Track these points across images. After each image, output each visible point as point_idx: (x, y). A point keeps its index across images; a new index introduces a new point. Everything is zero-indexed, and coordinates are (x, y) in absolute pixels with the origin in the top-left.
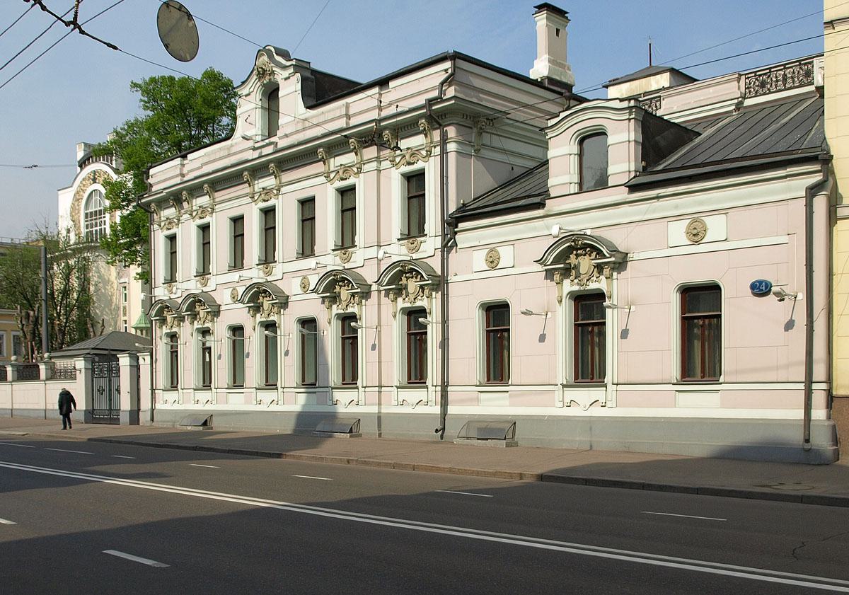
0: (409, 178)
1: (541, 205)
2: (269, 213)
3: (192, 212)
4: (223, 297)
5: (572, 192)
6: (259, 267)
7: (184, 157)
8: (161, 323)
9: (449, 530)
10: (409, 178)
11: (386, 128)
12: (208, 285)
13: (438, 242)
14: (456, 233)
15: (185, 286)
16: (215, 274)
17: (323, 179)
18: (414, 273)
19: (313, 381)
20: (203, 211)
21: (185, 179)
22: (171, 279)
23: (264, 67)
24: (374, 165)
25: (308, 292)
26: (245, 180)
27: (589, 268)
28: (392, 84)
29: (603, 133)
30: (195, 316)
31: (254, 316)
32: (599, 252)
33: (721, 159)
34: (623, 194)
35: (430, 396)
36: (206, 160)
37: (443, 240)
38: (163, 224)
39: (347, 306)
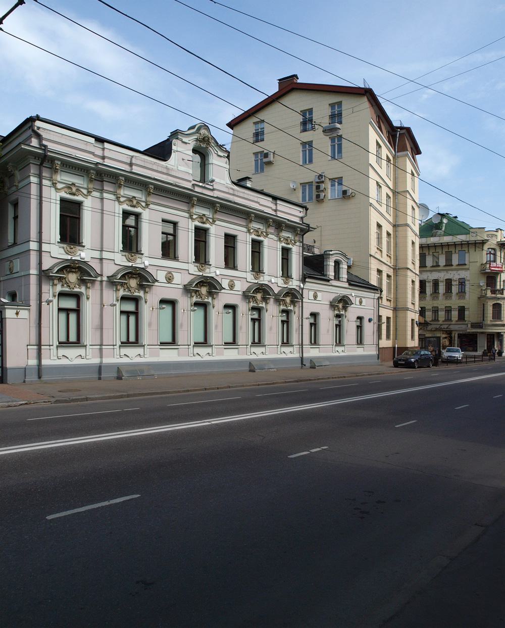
9: (6, 450)
34: (346, 285)
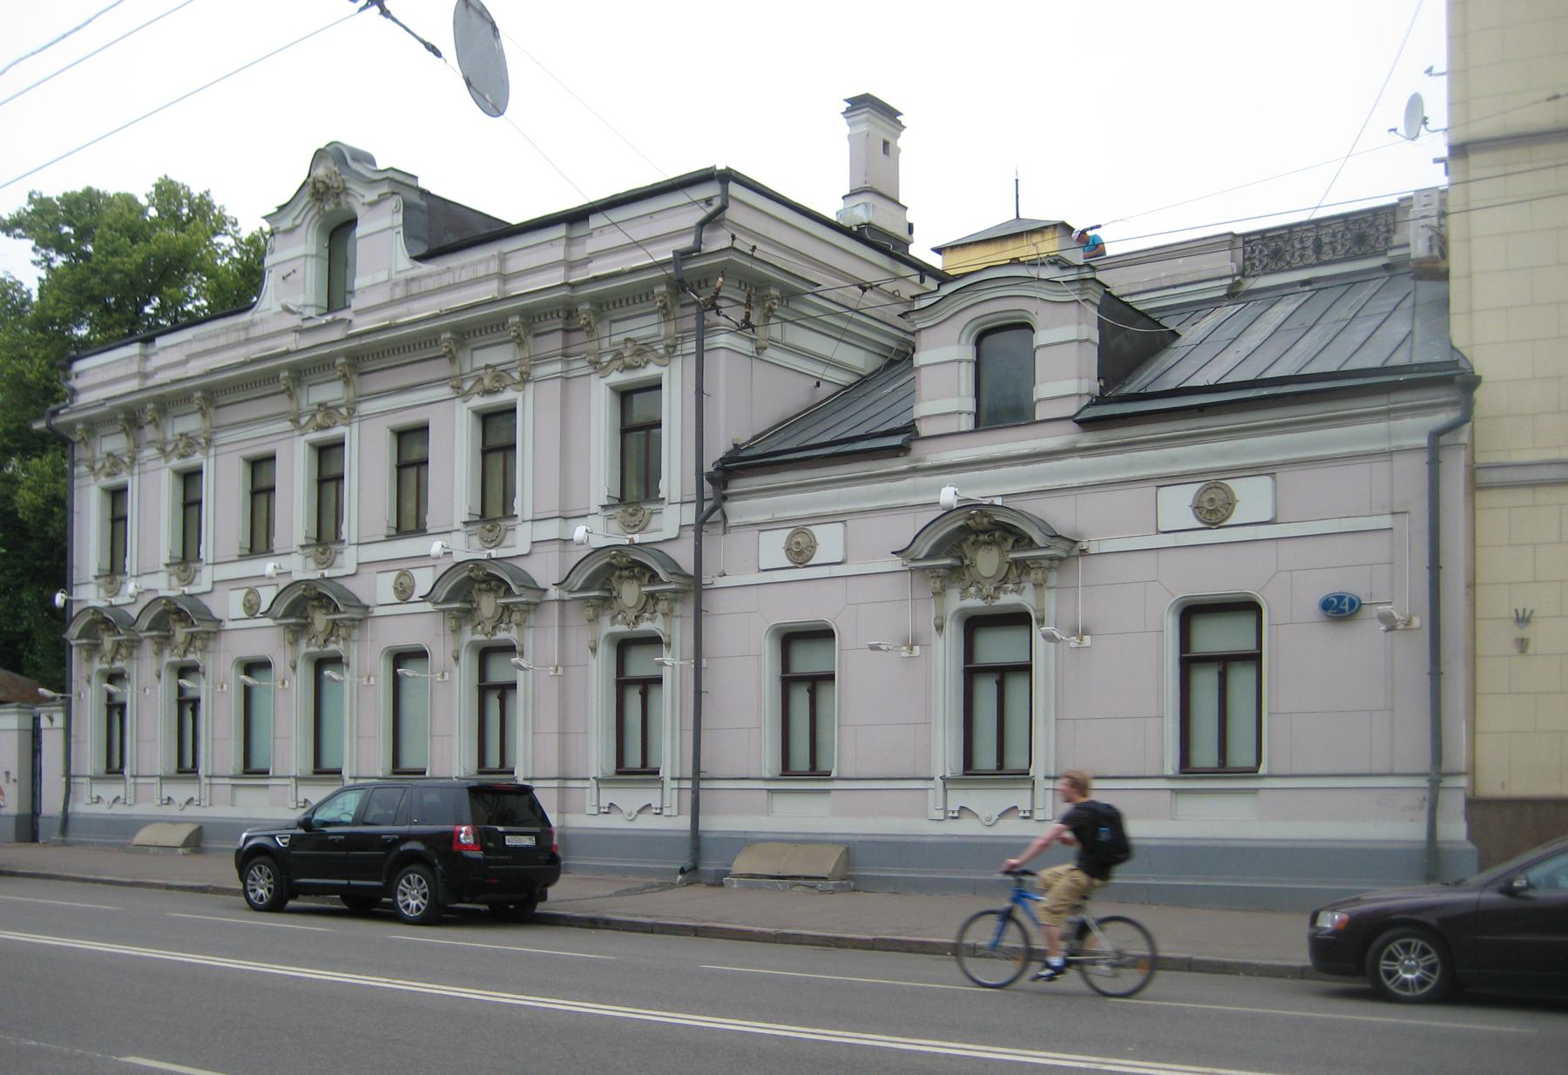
1: (901, 450)
2: (327, 453)
3: (94, 462)
4: (229, 606)
5: (963, 429)
6: (307, 551)
7: (148, 340)
8: (88, 651)
10: (625, 395)
11: (583, 300)
12: (335, 564)
13: (689, 514)
14: (725, 498)
15: (148, 582)
16: (211, 561)
17: (444, 392)
18: (324, 602)
19: (1252, 763)
20: (189, 443)
21: (150, 383)
22: (115, 568)
23: (327, 181)
24: (557, 367)
25: (258, 615)
26: (283, 387)
27: (639, 598)
28: (596, 221)
29: (1027, 327)
30: (165, 641)
32: (654, 578)
33: (1334, 369)
34: (1065, 437)
35: (667, 798)
36: (197, 347)
37: (699, 510)
38: (98, 466)
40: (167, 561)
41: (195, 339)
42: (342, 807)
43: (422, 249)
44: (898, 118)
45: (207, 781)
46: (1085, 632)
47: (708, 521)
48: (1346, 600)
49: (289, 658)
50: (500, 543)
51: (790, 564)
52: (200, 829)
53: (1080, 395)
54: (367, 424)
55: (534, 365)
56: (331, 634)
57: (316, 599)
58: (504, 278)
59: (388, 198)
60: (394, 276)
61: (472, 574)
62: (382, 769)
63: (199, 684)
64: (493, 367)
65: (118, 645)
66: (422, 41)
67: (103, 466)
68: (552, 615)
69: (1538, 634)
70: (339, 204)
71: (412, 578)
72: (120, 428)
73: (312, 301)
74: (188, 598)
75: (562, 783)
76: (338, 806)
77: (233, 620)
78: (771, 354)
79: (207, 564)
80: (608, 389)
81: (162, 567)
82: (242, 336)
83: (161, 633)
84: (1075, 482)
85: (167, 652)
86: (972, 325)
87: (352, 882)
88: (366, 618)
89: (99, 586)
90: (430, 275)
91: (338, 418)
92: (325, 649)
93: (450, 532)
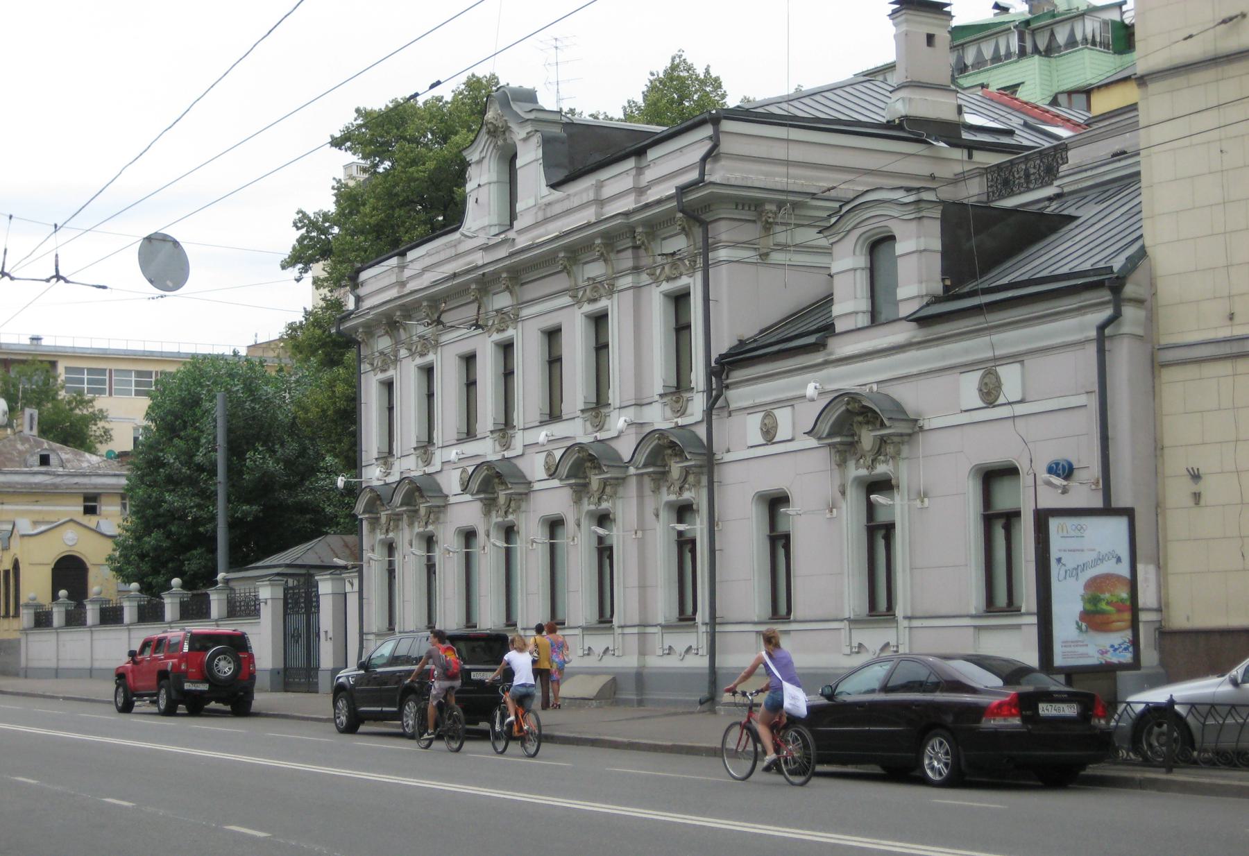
0: (382, 383)
1: (819, 346)
4: (535, 468)
5: (860, 326)
7: (403, 254)
10: (382, 383)
16: (618, 406)
17: (566, 300)
23: (495, 122)
31: (842, 464)
37: (709, 396)
39: (873, 461)
40: (582, 407)
41: (428, 254)
42: (895, 649)
43: (561, 175)
44: (947, 9)
45: (906, 623)
46: (926, 495)
47: (716, 406)
48: (1060, 466)
49: (837, 482)
50: (603, 427)
51: (983, 405)
52: (614, 680)
53: (922, 296)
54: (527, 323)
55: (617, 277)
56: (879, 452)
57: (861, 414)
58: (600, 202)
59: (533, 135)
60: (540, 201)
61: (849, 407)
62: (975, 608)
63: (893, 499)
64: (594, 279)
65: (687, 472)
66: (94, 286)
67: (493, 324)
68: (632, 487)
69: (1208, 487)
70: (505, 140)
71: (998, 379)
72: (383, 332)
73: (495, 221)
74: (599, 444)
75: (642, 630)
76: (892, 649)
77: (752, 447)
78: (777, 257)
79: (697, 392)
80: (662, 296)
81: (579, 413)
82: (452, 252)
83: (578, 481)
84: (914, 370)
85: (851, 464)
86: (865, 236)
87: (384, 709)
88: (445, 506)
89: (665, 404)
90: (557, 201)
91: (682, 269)
92: (506, 519)
93: (574, 418)
